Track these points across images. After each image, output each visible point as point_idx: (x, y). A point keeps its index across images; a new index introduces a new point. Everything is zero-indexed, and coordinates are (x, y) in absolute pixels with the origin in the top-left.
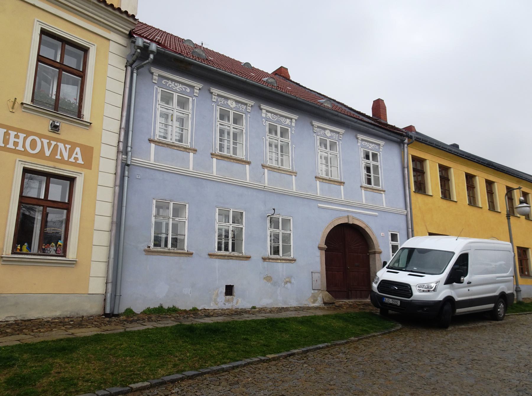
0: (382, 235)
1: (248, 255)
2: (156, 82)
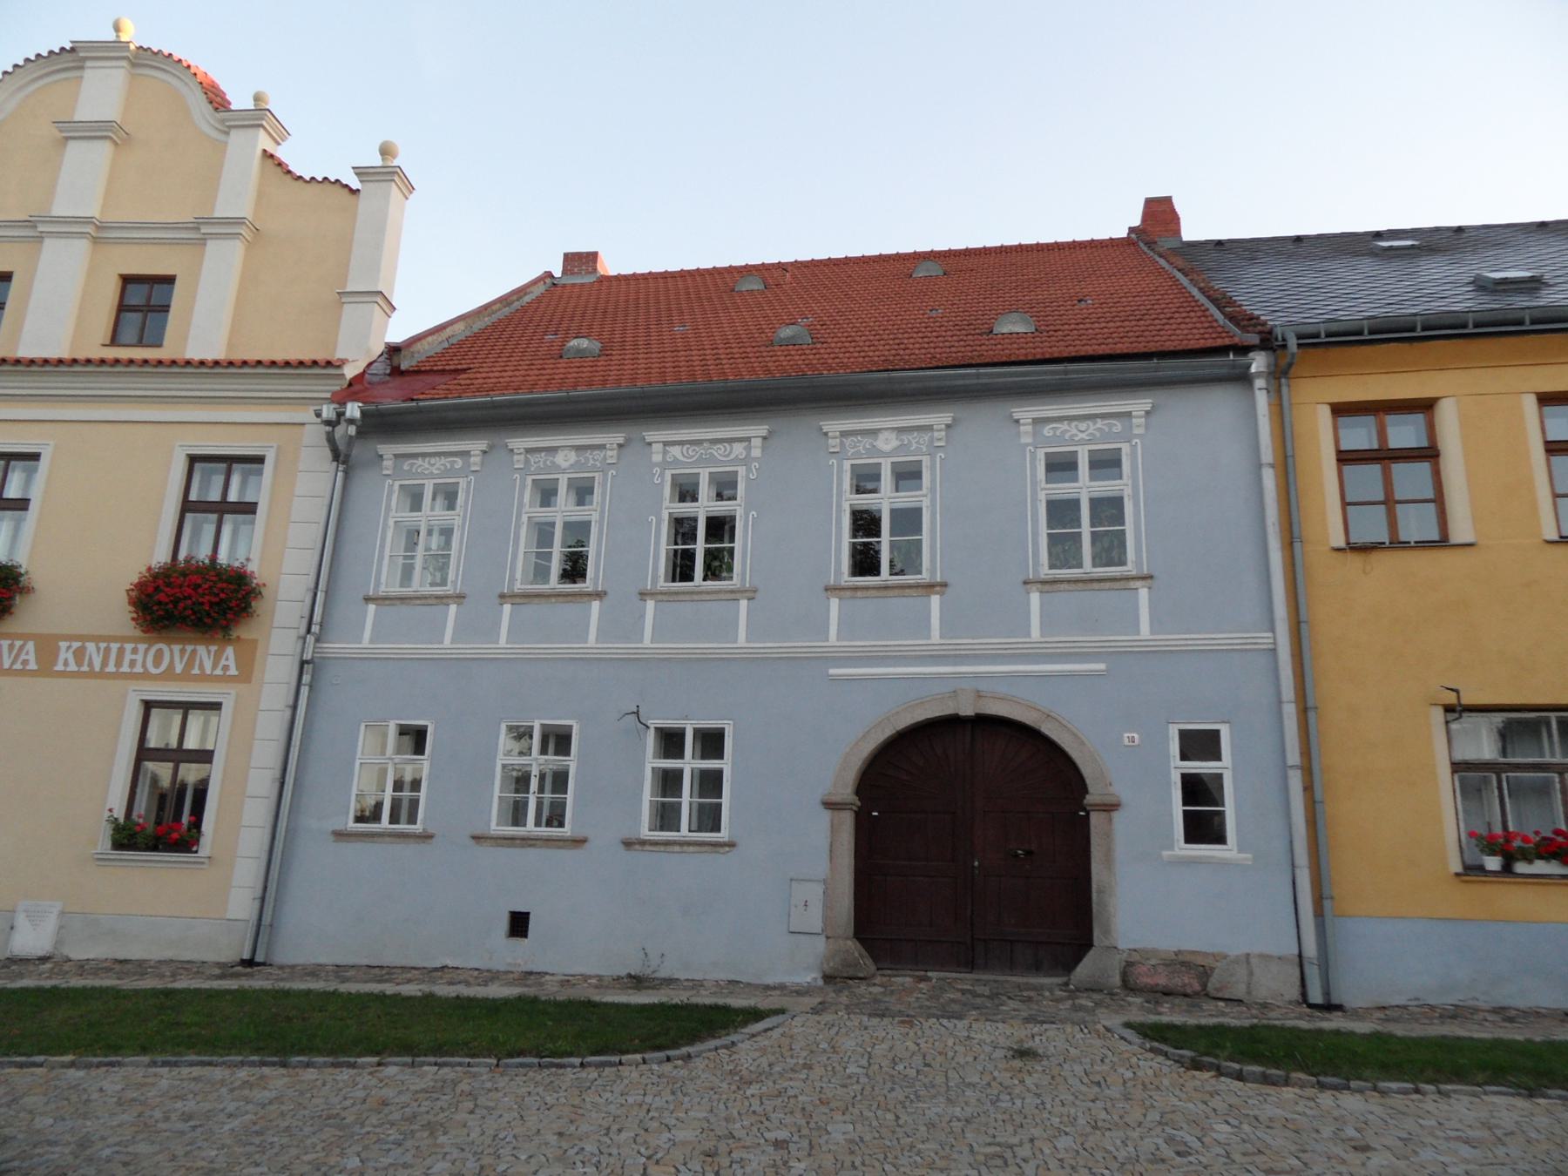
0: (1126, 742)
1: (580, 834)
2: (478, 469)
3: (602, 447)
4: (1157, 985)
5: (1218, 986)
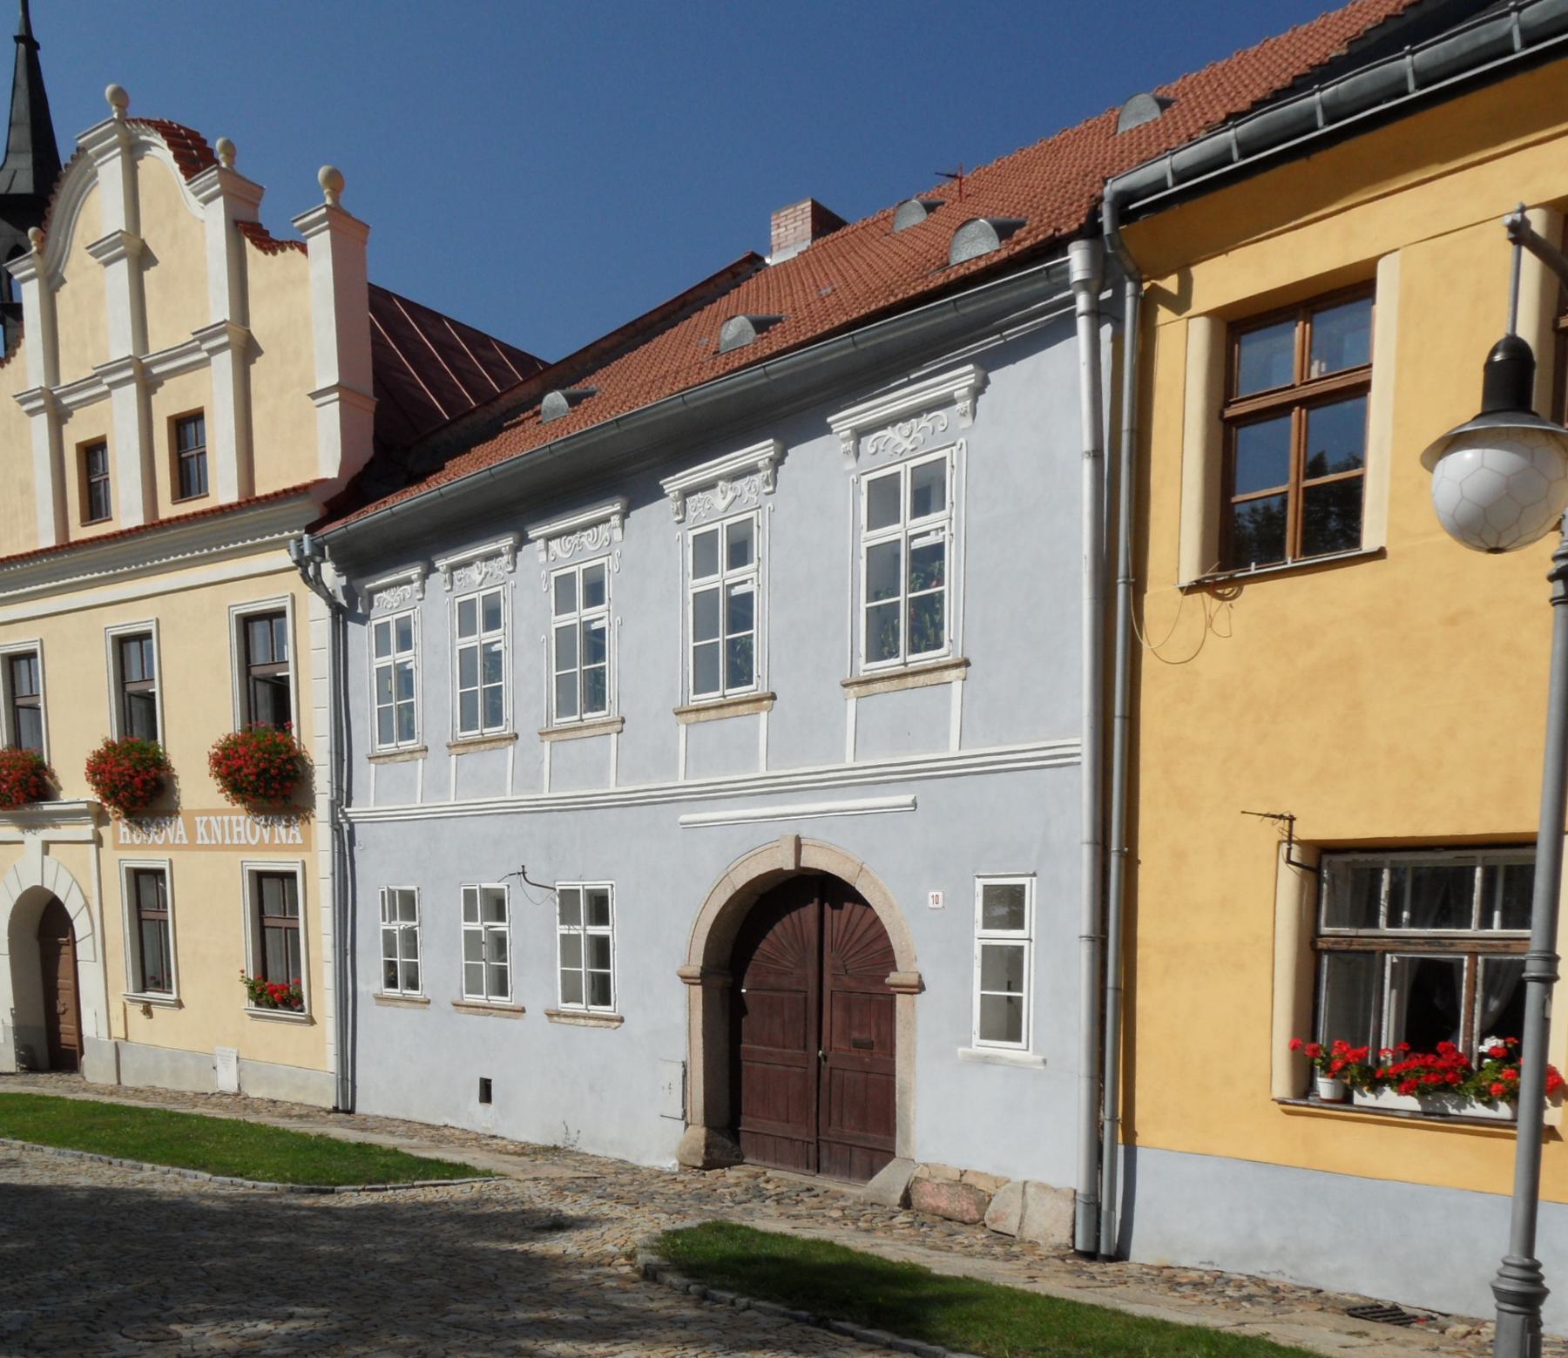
0: (931, 904)
3: (605, 520)
4: (938, 1207)
5: (993, 1216)
